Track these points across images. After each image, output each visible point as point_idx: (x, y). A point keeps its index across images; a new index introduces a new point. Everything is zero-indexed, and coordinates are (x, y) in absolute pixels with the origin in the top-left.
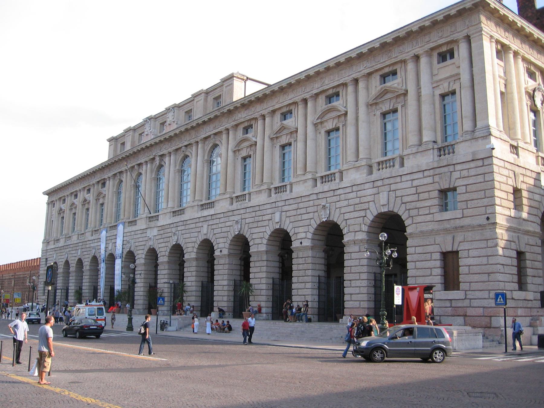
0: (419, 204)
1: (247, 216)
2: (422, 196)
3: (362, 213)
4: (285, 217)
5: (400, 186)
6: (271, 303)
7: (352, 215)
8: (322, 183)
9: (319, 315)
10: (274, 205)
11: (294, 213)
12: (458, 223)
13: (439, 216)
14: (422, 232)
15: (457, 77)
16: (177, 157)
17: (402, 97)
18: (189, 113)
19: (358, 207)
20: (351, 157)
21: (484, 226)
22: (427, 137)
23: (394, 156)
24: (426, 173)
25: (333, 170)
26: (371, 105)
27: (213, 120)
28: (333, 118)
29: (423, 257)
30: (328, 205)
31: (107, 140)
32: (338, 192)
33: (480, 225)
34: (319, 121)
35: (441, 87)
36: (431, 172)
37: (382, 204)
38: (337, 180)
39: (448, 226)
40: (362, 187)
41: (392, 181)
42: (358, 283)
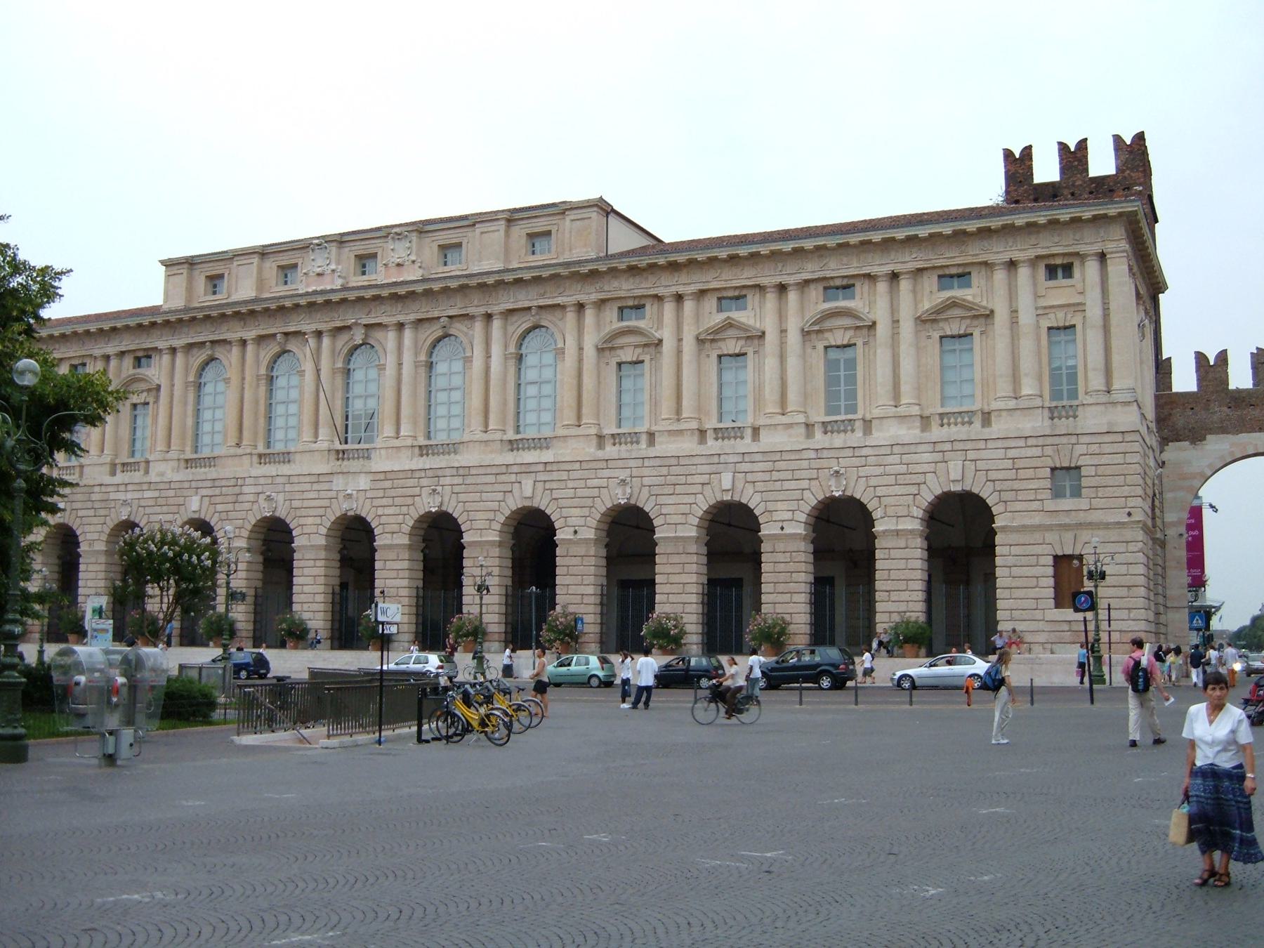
0: (1016, 485)
1: (646, 472)
2: (1022, 474)
3: (914, 490)
4: (742, 482)
5: (984, 454)
6: (503, 626)
7: (891, 490)
8: (942, 425)
9: (332, 638)
10: (716, 459)
11: (766, 476)
12: (1082, 517)
13: (1050, 505)
14: (1024, 526)
15: (1079, 308)
16: (511, 329)
17: (756, 342)
18: (214, 281)
19: (901, 479)
20: (666, 410)
21: (1123, 523)
22: (1027, 389)
23: (974, 408)
24: (1031, 442)
25: (138, 458)
26: (924, 322)
27: (568, 274)
28: (636, 346)
29: (1024, 560)
30: (439, 489)
31: (1030, 147)
32: (865, 452)
33: (1118, 523)
34: (816, 328)
35: (1052, 316)
36: (1041, 441)
37: (952, 478)
38: (142, 472)
39: (1067, 521)
40: (913, 449)
41: (969, 445)
42: (905, 596)
